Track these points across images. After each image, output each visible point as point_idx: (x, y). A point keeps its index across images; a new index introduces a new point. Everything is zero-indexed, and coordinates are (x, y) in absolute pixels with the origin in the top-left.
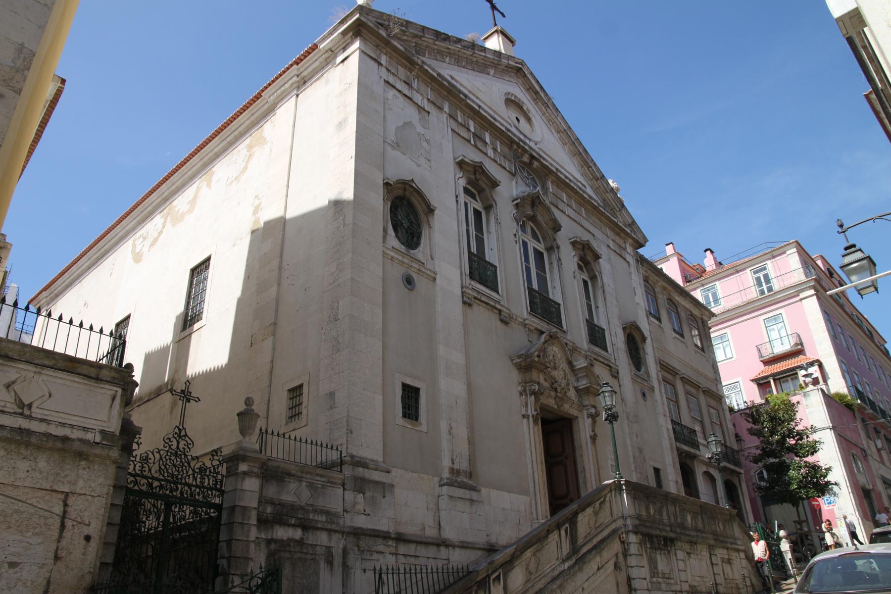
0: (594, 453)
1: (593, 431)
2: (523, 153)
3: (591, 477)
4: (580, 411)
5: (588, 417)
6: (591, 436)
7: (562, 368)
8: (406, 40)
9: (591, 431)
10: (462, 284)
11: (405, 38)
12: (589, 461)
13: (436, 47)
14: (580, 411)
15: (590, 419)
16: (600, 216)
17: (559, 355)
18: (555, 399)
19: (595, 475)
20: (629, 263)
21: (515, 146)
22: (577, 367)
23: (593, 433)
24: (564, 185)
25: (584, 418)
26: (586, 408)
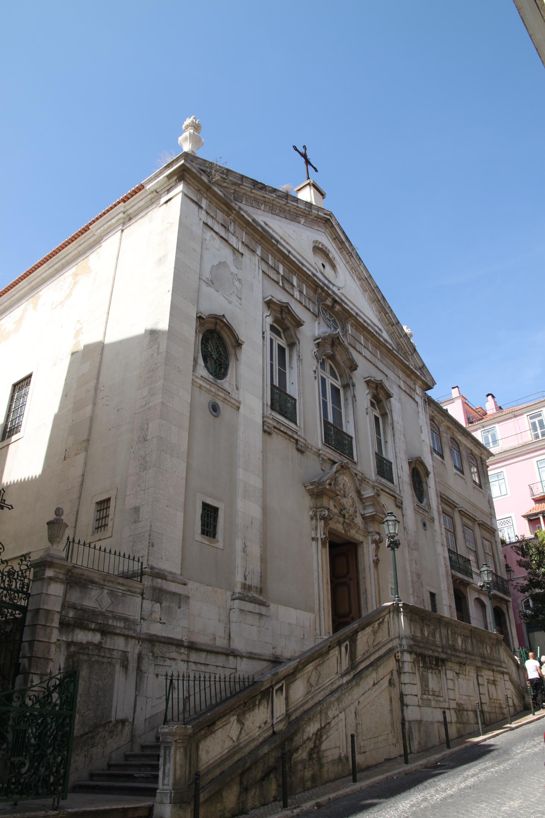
0: (376, 576)
1: (376, 556)
2: (326, 296)
3: (372, 598)
4: (366, 537)
5: (372, 543)
6: (374, 561)
7: (351, 497)
8: (225, 187)
9: (374, 555)
10: (263, 414)
11: (225, 184)
12: (371, 584)
13: (253, 195)
14: (366, 537)
15: (374, 545)
16: (393, 358)
17: (349, 484)
18: (343, 524)
19: (376, 596)
20: (417, 403)
21: (320, 290)
22: (365, 497)
23: (376, 558)
24: (363, 329)
25: (368, 543)
26: (371, 534)
